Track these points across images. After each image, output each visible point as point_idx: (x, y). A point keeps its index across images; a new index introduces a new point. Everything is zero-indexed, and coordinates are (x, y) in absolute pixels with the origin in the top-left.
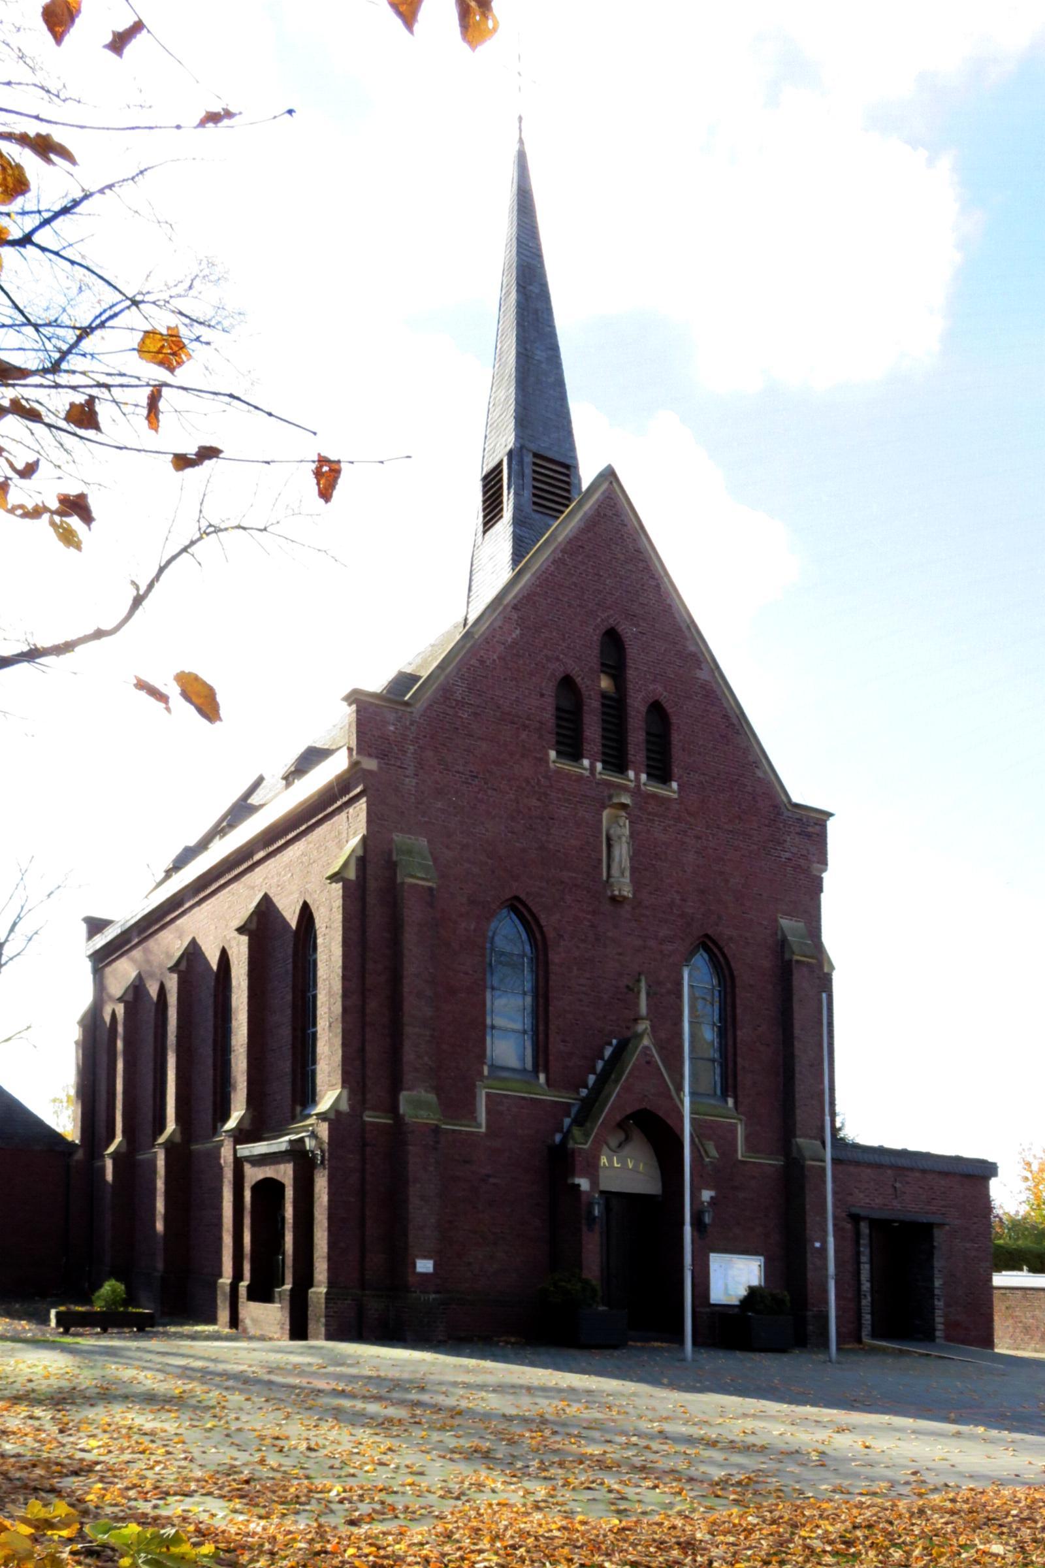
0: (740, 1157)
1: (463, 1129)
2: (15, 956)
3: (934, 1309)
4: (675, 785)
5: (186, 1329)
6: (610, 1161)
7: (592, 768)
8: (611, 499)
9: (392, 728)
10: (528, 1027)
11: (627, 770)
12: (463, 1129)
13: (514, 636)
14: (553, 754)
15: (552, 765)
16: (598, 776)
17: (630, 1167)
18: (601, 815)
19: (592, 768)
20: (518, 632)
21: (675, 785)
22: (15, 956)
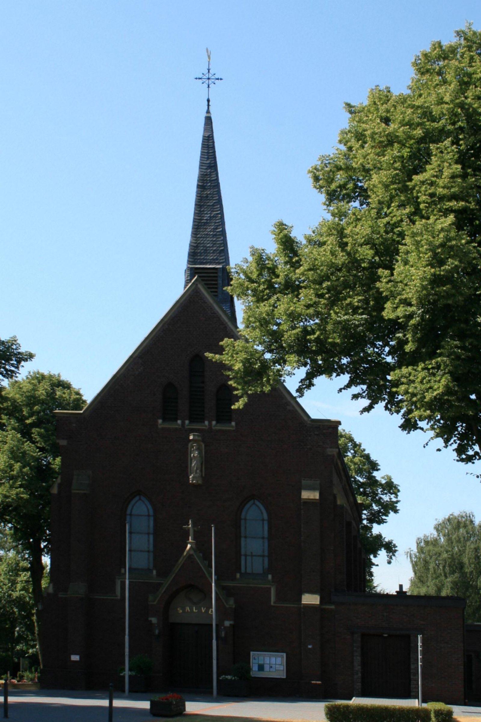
0: (272, 604)
1: (109, 598)
2: (208, 108)
3: (410, 680)
4: (233, 424)
5: (329, 700)
6: (191, 609)
7: (183, 423)
8: (198, 292)
9: (74, 425)
10: (151, 548)
11: (433, 268)
12: (109, 598)
13: (140, 370)
14: (160, 421)
15: (160, 427)
16: (186, 427)
17: (203, 611)
18: (188, 445)
19: (183, 423)
20: (142, 368)
21: (233, 424)
22: (208, 108)
